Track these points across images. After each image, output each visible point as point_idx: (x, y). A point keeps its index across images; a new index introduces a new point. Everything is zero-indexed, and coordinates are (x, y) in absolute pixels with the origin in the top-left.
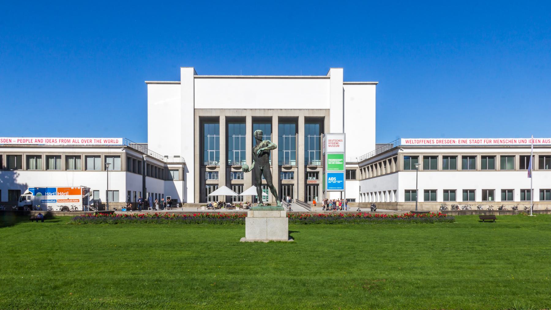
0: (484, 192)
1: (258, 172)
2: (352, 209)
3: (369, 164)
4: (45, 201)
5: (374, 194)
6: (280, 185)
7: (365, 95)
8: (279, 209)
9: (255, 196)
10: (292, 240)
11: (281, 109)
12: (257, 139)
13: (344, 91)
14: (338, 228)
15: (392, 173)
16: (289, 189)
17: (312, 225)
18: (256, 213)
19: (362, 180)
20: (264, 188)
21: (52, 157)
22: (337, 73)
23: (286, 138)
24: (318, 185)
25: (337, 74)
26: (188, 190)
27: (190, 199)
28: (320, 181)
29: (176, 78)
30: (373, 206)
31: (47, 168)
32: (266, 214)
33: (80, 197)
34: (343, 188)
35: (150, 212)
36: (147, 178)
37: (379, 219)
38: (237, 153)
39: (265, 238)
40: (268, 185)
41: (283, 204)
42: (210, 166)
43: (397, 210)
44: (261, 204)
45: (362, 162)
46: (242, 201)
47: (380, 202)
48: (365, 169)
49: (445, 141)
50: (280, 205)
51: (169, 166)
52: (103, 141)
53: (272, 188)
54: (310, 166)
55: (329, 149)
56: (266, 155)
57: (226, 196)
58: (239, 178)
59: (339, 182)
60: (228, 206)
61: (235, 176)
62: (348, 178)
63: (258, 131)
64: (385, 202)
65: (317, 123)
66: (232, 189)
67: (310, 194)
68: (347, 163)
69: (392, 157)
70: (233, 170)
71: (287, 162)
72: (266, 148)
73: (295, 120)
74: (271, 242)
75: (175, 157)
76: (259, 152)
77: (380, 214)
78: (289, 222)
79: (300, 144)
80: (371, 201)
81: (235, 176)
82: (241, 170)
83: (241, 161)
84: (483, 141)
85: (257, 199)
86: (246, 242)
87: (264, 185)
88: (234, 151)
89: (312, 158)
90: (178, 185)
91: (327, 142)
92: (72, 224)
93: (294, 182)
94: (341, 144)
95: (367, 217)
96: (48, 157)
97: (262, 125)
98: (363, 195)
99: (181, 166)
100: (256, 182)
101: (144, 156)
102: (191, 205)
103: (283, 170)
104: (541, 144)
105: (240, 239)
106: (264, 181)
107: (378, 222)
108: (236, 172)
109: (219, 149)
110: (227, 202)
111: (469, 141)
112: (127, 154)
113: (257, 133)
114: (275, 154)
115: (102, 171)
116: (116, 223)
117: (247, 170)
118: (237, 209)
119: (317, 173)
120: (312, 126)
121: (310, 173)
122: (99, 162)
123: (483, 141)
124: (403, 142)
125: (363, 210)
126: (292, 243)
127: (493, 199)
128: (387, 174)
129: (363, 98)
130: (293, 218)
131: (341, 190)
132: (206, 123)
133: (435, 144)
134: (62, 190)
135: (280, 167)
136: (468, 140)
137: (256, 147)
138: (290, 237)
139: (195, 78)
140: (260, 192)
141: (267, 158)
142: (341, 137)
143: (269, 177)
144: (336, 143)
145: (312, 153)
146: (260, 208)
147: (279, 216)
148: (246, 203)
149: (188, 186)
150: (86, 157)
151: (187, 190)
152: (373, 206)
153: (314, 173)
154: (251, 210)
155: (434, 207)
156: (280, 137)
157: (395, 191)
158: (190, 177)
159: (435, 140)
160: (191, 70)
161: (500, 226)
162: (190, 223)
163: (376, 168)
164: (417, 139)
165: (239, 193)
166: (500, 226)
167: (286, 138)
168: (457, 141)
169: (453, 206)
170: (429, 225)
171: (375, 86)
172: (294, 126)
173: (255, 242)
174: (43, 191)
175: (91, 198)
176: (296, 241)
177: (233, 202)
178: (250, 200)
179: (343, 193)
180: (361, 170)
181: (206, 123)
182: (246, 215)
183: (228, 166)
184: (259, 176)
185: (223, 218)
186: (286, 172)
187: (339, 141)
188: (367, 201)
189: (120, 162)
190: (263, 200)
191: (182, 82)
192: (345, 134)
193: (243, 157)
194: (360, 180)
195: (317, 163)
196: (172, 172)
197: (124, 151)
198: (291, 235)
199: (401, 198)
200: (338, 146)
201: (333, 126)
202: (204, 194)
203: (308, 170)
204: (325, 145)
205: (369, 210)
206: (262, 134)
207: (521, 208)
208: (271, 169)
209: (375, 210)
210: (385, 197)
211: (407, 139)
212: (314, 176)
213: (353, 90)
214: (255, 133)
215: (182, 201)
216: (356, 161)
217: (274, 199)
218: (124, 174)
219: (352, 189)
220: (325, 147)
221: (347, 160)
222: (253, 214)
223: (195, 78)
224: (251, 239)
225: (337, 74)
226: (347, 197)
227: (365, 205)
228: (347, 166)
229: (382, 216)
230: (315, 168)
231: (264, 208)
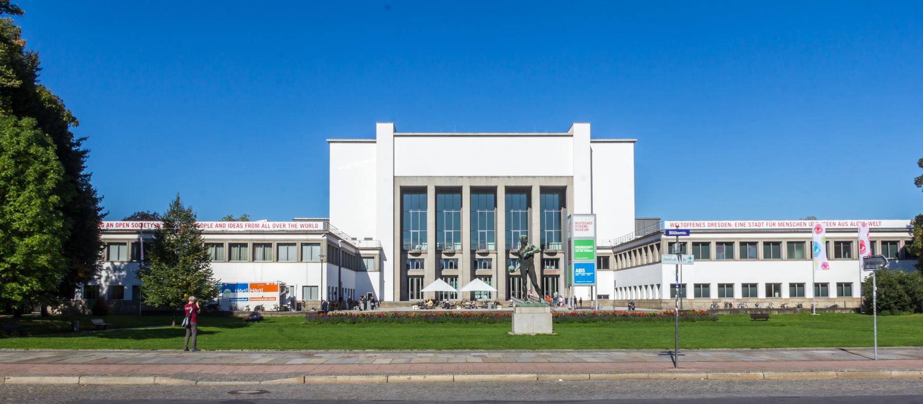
0: (768, 286)
2: (608, 308)
3: (626, 250)
4: (235, 299)
5: (633, 289)
6: (543, 276)
7: (619, 158)
15: (654, 263)
18: (524, 310)
21: (235, 245)
22: (582, 130)
24: (558, 276)
27: (389, 296)
28: (561, 272)
29: (370, 136)
30: (631, 304)
31: (254, 259)
33: (277, 295)
35: (355, 311)
36: (342, 269)
42: (413, 251)
43: (661, 309)
48: (621, 256)
49: (718, 224)
51: (361, 252)
52: (299, 226)
54: (548, 251)
55: (577, 234)
59: (589, 274)
65: (557, 195)
68: (599, 248)
70: (410, 257)
73: (527, 190)
75: (366, 239)
79: (534, 222)
84: (765, 224)
90: (374, 277)
96: (231, 245)
99: (377, 252)
104: (837, 227)
107: (636, 321)
109: (426, 229)
111: (748, 224)
112: (328, 241)
119: (557, 260)
120: (550, 196)
121: (548, 260)
123: (765, 224)
124: (667, 225)
125: (617, 309)
127: (780, 295)
128: (648, 264)
132: (410, 194)
133: (706, 227)
134: (255, 286)
135: (507, 252)
136: (747, 222)
139: (395, 136)
142: (591, 219)
144: (585, 227)
145: (550, 234)
150: (278, 245)
151: (385, 285)
153: (552, 260)
155: (703, 305)
157: (659, 286)
158: (388, 266)
159: (706, 222)
160: (390, 126)
161: (773, 325)
162: (433, 322)
166: (773, 325)
168: (733, 224)
169: (726, 305)
174: (233, 287)
175: (288, 296)
180: (616, 257)
181: (410, 194)
183: (438, 252)
191: (378, 140)
192: (595, 215)
195: (555, 247)
196: (365, 260)
199: (666, 294)
201: (578, 203)
202: (409, 286)
203: (545, 256)
207: (764, 306)
210: (654, 293)
212: (552, 264)
213: (604, 150)
215: (378, 299)
216: (609, 245)
219: (606, 281)
221: (599, 245)
223: (395, 136)
226: (599, 293)
227: (622, 303)
228: (599, 251)
229: (639, 315)
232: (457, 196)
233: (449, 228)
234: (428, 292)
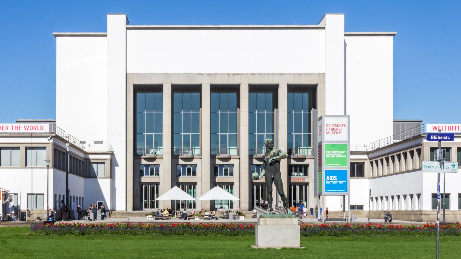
3: (384, 156)
11: (253, 74)
13: (345, 45)
14: (345, 240)
15: (414, 170)
17: (313, 237)
18: (269, 221)
19: (374, 178)
24: (307, 184)
25: (335, 22)
26: (116, 191)
28: (310, 179)
29: (100, 29)
30: (388, 216)
32: (278, 221)
34: (346, 191)
36: (70, 175)
37: (393, 231)
38: (187, 137)
39: (278, 244)
43: (421, 221)
45: (373, 152)
47: (399, 211)
48: (377, 162)
51: (91, 157)
54: (296, 156)
55: (328, 138)
59: (341, 182)
62: (353, 175)
64: (406, 211)
65: (306, 94)
68: (352, 153)
69: (415, 149)
70: (144, 162)
72: (278, 157)
74: (284, 249)
75: (96, 142)
77: (395, 225)
80: (386, 209)
83: (156, 148)
88: (183, 134)
89: (298, 145)
90: (104, 184)
91: (325, 128)
92: (32, 235)
94: (344, 130)
95: (379, 228)
98: (374, 199)
99: (108, 157)
101: (67, 145)
102: (122, 214)
108: (186, 165)
109: (161, 131)
112: (55, 145)
115: (22, 167)
116: (83, 235)
119: (306, 166)
120: (298, 95)
121: (296, 166)
122: (18, 155)
129: (376, 53)
131: (344, 194)
132: (144, 93)
135: (251, 157)
139: (127, 29)
142: (344, 121)
144: (337, 129)
146: (271, 215)
147: (290, 223)
149: (116, 187)
152: (388, 215)
153: (300, 166)
157: (419, 195)
158: (120, 172)
160: (122, 18)
162: (169, 234)
163: (393, 161)
164: (448, 125)
167: (222, 114)
170: (453, 237)
171: (391, 38)
175: (11, 204)
179: (347, 197)
180: (372, 163)
181: (144, 93)
183: (175, 157)
185: (207, 229)
187: (342, 126)
188: (380, 209)
189: (46, 156)
191: (108, 33)
192: (349, 117)
194: (370, 178)
196: (95, 166)
197: (51, 141)
199: (426, 205)
200: (340, 133)
201: (329, 103)
203: (293, 162)
204: (321, 131)
205: (383, 221)
209: (390, 221)
211: (434, 125)
212: (300, 171)
215: (109, 208)
216: (364, 150)
218: (51, 171)
219: (360, 190)
220: (321, 134)
221: (353, 149)
222: (265, 221)
223: (127, 29)
225: (335, 22)
226: (352, 203)
227: (377, 214)
228: (353, 157)
230: (303, 159)
231: (275, 215)
232: (196, 95)
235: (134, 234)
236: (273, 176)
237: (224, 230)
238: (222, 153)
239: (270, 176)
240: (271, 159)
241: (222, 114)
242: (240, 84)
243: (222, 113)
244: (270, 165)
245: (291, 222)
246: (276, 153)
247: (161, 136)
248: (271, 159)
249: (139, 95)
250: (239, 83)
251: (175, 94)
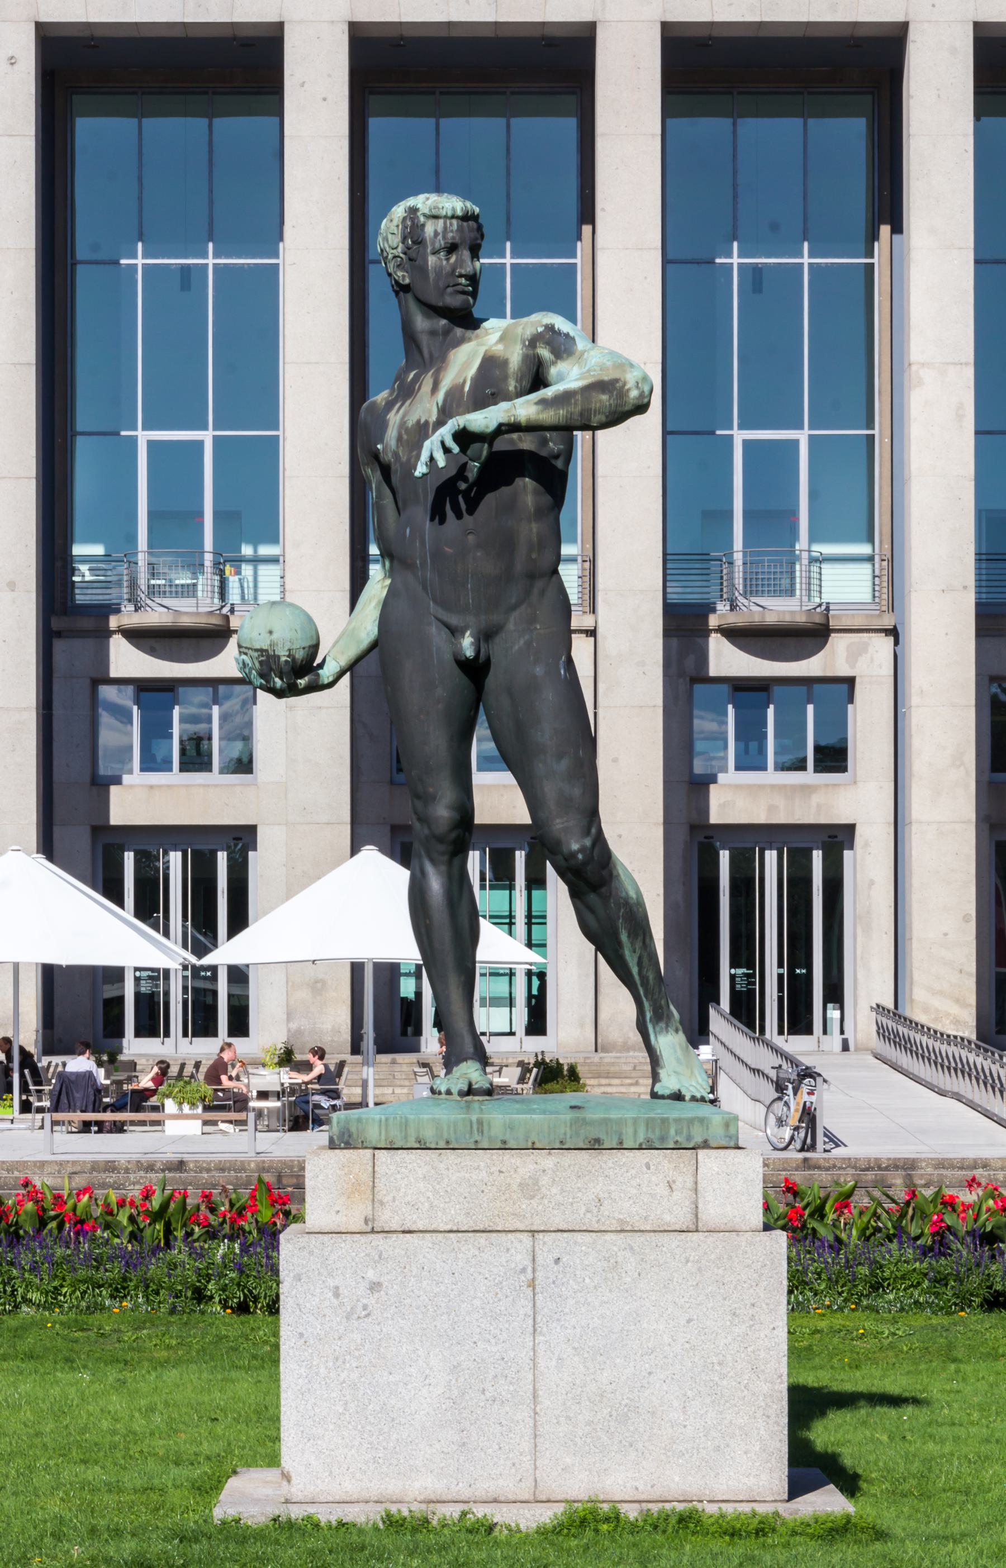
1: (428, 697)
6: (695, 840)
8: (680, 1129)
9: (389, 973)
10: (827, 1502)
12: (410, 306)
16: (797, 887)
18: (413, 1183)
20: (501, 875)
23: (755, 277)
24: (838, 838)
32: (530, 1188)
38: (175, 465)
40: (540, 843)
41: (728, 1066)
44: (469, 1071)
46: (239, 1026)
50: (696, 1085)
53: (593, 879)
56: (526, 487)
57: (49, 973)
58: (196, 757)
60: (70, 1093)
61: (155, 730)
63: (423, 202)
66: (113, 892)
67: (745, 950)
70: (127, 660)
71: (775, 573)
72: (524, 409)
74: (587, 1524)
76: (434, 451)
78: (797, 1282)
81: (155, 730)
82: (225, 664)
83: (227, 559)
85: (411, 1010)
86: (285, 1529)
87: (500, 843)
88: (143, 437)
93: (855, 799)
97: (475, 134)
100: (401, 803)
103: (726, 660)
105: (209, 1488)
106: (498, 798)
109: (268, 413)
110: (55, 1040)
113: (412, 230)
114: (624, 476)
117: (294, 674)
118: (181, 1131)
126: (838, 1531)
130: (845, 1241)
135: (684, 626)
137: (406, 392)
138: (810, 1466)
140: (447, 932)
141: (530, 530)
143: (561, 750)
146: (449, 1114)
147: (679, 1216)
148: (287, 1059)
154: (344, 1141)
156: (684, 262)
165: (203, 931)
167: (755, 277)
172: (850, 132)
173: (393, 1523)
176: (887, 1517)
177: (135, 1047)
178: (333, 1021)
182: (278, 1199)
184: (434, 741)
186: (753, 682)
190: (489, 1019)
193: (253, 512)
198: (824, 1434)
206: (472, 236)
208: (581, 649)
214: (388, 231)
217: (620, 1005)
224: (348, 1486)
231: (496, 1115)
233: (175, 406)
234: (305, 973)
235: (844, 1159)
236: (467, 644)
237: (179, 1253)
238: (752, 589)
239: (437, 636)
240: (446, 432)
241: (755, 278)
242: (903, 27)
243: (757, 269)
244: (437, 513)
245: (682, 1197)
246: (515, 356)
247: (268, 452)
248: (446, 432)
249: (93, 132)
250: (586, 17)
251: (375, 124)
